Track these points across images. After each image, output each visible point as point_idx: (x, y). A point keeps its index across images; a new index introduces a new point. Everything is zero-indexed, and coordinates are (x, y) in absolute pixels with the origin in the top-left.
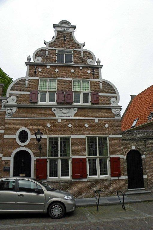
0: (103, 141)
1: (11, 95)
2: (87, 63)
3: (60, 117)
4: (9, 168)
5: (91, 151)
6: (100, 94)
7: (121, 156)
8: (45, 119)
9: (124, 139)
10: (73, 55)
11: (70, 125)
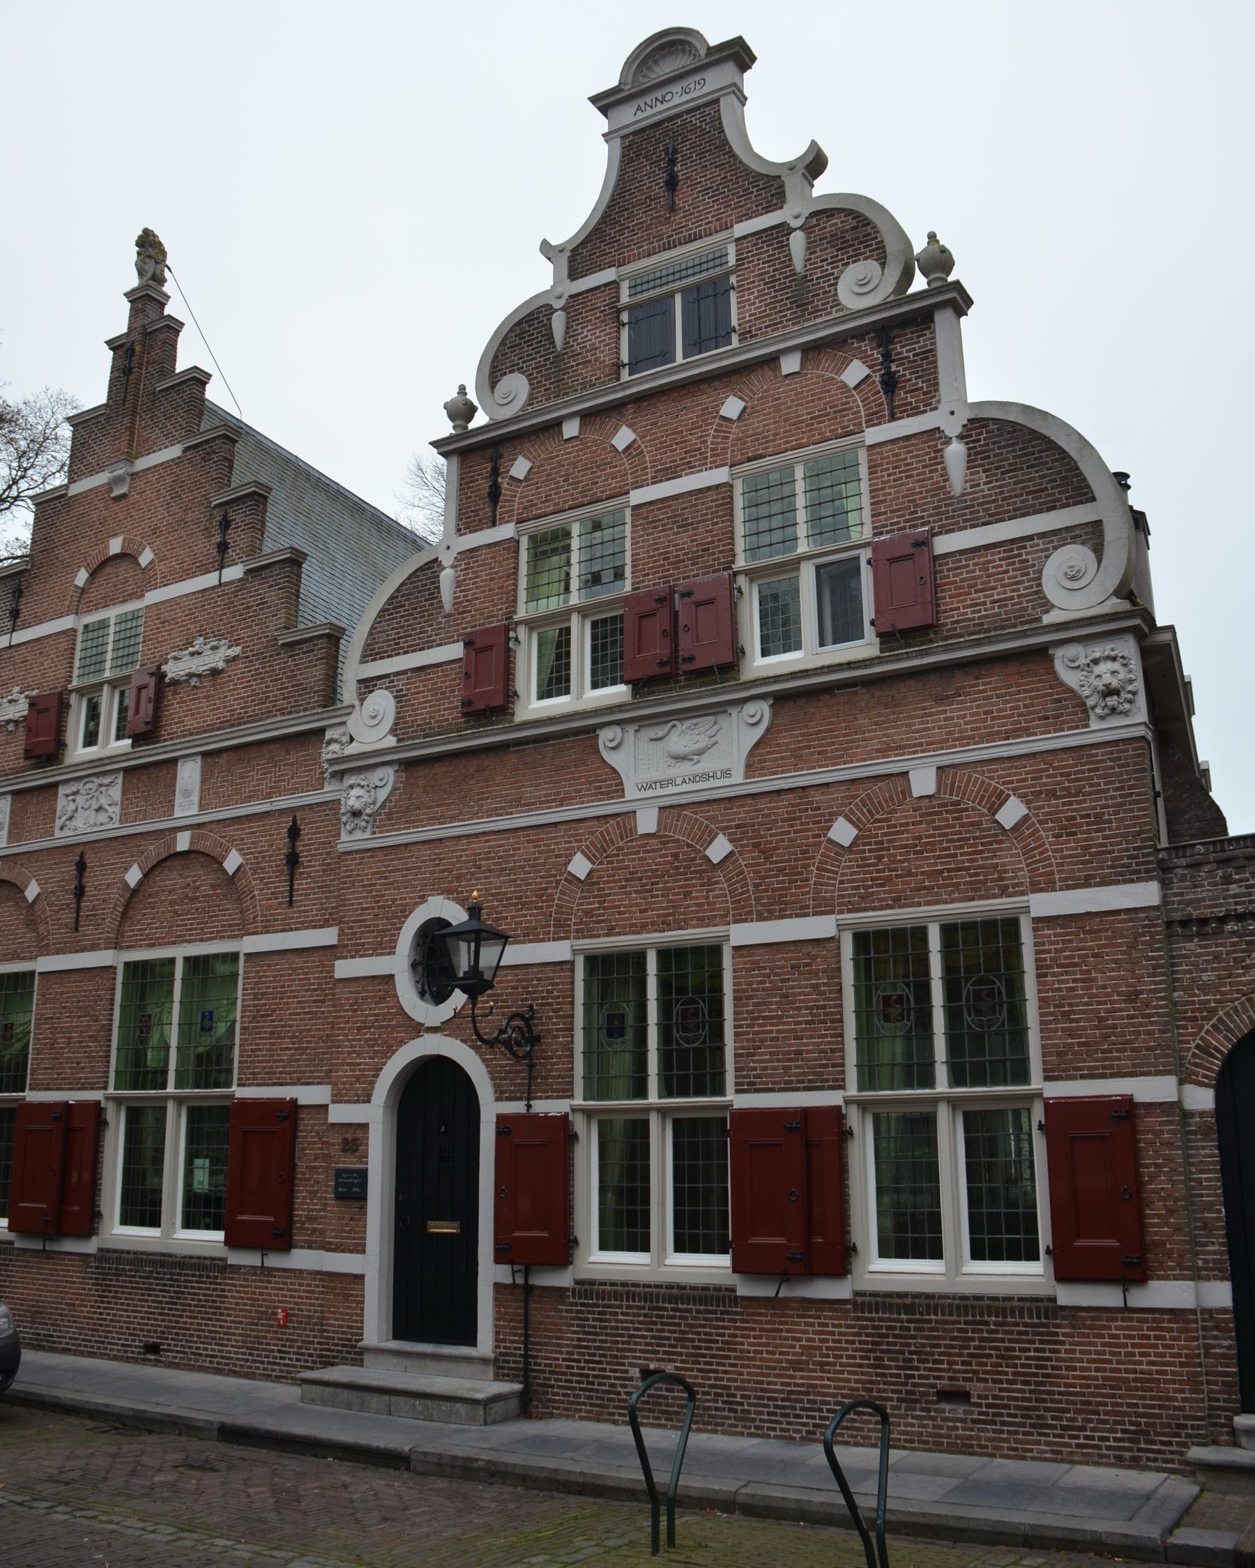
0: (986, 953)
1: (367, 685)
2: (837, 304)
3: (650, 793)
4: (364, 1174)
5: (683, 1053)
6: (945, 544)
7: (1152, 1089)
8: (555, 824)
9: (1185, 923)
10: (733, 279)
11: (719, 849)
